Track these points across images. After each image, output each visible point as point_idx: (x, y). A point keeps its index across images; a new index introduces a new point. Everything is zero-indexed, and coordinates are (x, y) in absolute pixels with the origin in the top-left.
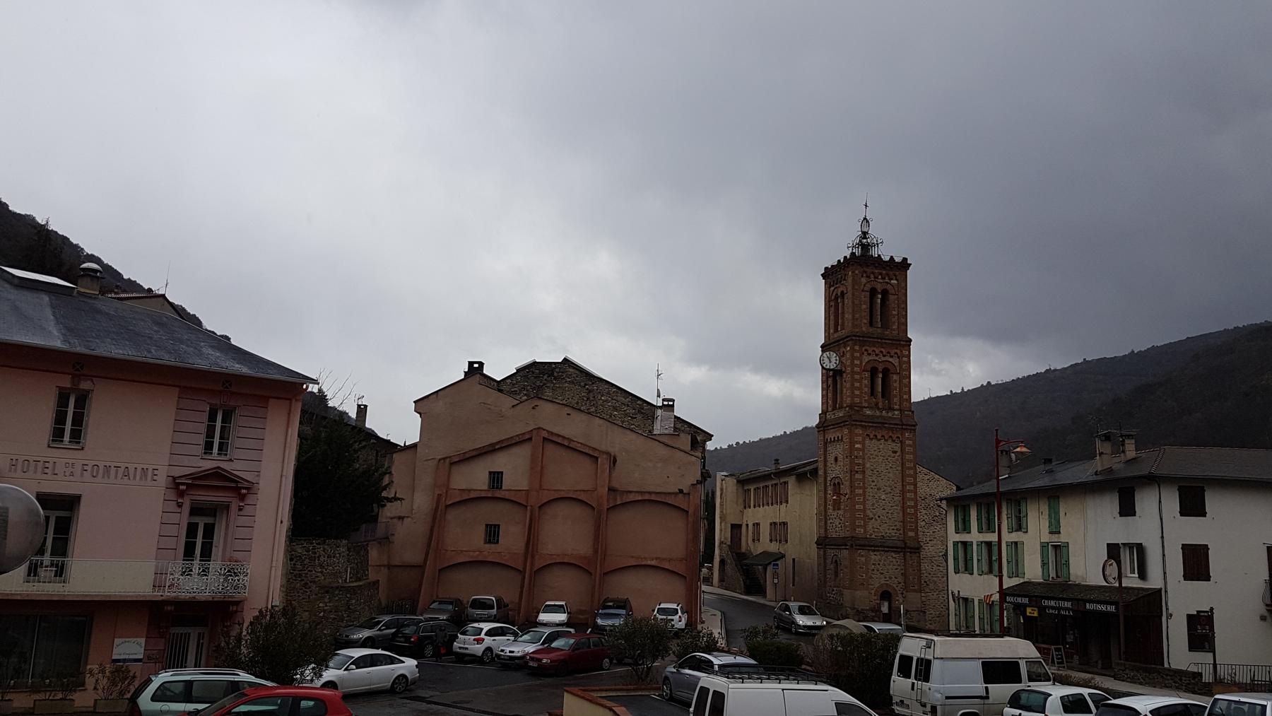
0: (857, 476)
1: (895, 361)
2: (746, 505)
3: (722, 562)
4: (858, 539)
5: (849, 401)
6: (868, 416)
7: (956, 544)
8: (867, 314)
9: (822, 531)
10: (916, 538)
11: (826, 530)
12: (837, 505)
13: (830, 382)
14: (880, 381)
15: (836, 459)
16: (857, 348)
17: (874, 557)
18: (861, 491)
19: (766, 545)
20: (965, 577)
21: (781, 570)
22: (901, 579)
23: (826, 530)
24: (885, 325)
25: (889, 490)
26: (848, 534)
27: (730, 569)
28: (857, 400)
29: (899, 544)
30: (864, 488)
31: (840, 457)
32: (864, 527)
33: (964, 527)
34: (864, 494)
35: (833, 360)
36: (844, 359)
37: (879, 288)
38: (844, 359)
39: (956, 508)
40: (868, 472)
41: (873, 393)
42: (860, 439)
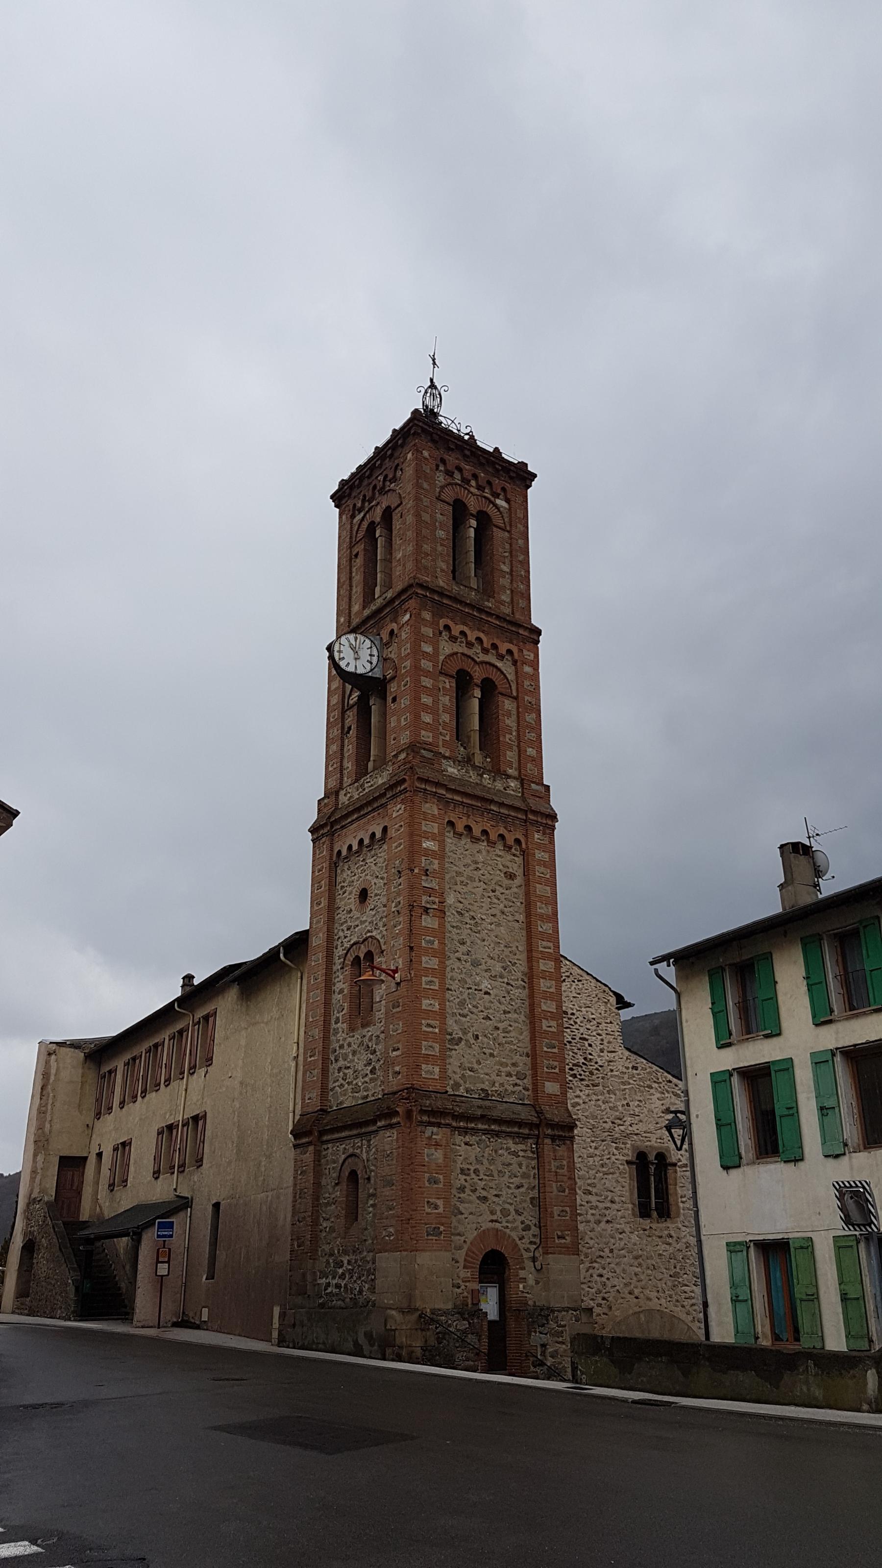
0: (428, 922)
1: (506, 667)
2: (101, 1109)
3: (29, 1248)
4: (427, 1094)
5: (405, 739)
6: (452, 779)
7: (720, 1080)
8: (444, 550)
9: (315, 1094)
10: (561, 1100)
11: (324, 1090)
12: (361, 1010)
13: (351, 718)
14: (476, 703)
15: (363, 895)
16: (427, 615)
17: (468, 1150)
18: (434, 963)
19: (146, 1187)
20: (772, 1173)
21: (179, 1239)
22: (529, 1217)
23: (324, 1090)
24: (488, 589)
25: (498, 968)
26: (395, 1083)
27: (42, 1263)
28: (426, 736)
29: (526, 1114)
30: (442, 955)
31: (376, 887)
32: (442, 1060)
33: (755, 1016)
34: (441, 973)
35: (365, 654)
36: (392, 653)
37: (473, 504)
38: (392, 653)
39: (715, 977)
40: (451, 918)
41: (460, 733)
42: (434, 828)
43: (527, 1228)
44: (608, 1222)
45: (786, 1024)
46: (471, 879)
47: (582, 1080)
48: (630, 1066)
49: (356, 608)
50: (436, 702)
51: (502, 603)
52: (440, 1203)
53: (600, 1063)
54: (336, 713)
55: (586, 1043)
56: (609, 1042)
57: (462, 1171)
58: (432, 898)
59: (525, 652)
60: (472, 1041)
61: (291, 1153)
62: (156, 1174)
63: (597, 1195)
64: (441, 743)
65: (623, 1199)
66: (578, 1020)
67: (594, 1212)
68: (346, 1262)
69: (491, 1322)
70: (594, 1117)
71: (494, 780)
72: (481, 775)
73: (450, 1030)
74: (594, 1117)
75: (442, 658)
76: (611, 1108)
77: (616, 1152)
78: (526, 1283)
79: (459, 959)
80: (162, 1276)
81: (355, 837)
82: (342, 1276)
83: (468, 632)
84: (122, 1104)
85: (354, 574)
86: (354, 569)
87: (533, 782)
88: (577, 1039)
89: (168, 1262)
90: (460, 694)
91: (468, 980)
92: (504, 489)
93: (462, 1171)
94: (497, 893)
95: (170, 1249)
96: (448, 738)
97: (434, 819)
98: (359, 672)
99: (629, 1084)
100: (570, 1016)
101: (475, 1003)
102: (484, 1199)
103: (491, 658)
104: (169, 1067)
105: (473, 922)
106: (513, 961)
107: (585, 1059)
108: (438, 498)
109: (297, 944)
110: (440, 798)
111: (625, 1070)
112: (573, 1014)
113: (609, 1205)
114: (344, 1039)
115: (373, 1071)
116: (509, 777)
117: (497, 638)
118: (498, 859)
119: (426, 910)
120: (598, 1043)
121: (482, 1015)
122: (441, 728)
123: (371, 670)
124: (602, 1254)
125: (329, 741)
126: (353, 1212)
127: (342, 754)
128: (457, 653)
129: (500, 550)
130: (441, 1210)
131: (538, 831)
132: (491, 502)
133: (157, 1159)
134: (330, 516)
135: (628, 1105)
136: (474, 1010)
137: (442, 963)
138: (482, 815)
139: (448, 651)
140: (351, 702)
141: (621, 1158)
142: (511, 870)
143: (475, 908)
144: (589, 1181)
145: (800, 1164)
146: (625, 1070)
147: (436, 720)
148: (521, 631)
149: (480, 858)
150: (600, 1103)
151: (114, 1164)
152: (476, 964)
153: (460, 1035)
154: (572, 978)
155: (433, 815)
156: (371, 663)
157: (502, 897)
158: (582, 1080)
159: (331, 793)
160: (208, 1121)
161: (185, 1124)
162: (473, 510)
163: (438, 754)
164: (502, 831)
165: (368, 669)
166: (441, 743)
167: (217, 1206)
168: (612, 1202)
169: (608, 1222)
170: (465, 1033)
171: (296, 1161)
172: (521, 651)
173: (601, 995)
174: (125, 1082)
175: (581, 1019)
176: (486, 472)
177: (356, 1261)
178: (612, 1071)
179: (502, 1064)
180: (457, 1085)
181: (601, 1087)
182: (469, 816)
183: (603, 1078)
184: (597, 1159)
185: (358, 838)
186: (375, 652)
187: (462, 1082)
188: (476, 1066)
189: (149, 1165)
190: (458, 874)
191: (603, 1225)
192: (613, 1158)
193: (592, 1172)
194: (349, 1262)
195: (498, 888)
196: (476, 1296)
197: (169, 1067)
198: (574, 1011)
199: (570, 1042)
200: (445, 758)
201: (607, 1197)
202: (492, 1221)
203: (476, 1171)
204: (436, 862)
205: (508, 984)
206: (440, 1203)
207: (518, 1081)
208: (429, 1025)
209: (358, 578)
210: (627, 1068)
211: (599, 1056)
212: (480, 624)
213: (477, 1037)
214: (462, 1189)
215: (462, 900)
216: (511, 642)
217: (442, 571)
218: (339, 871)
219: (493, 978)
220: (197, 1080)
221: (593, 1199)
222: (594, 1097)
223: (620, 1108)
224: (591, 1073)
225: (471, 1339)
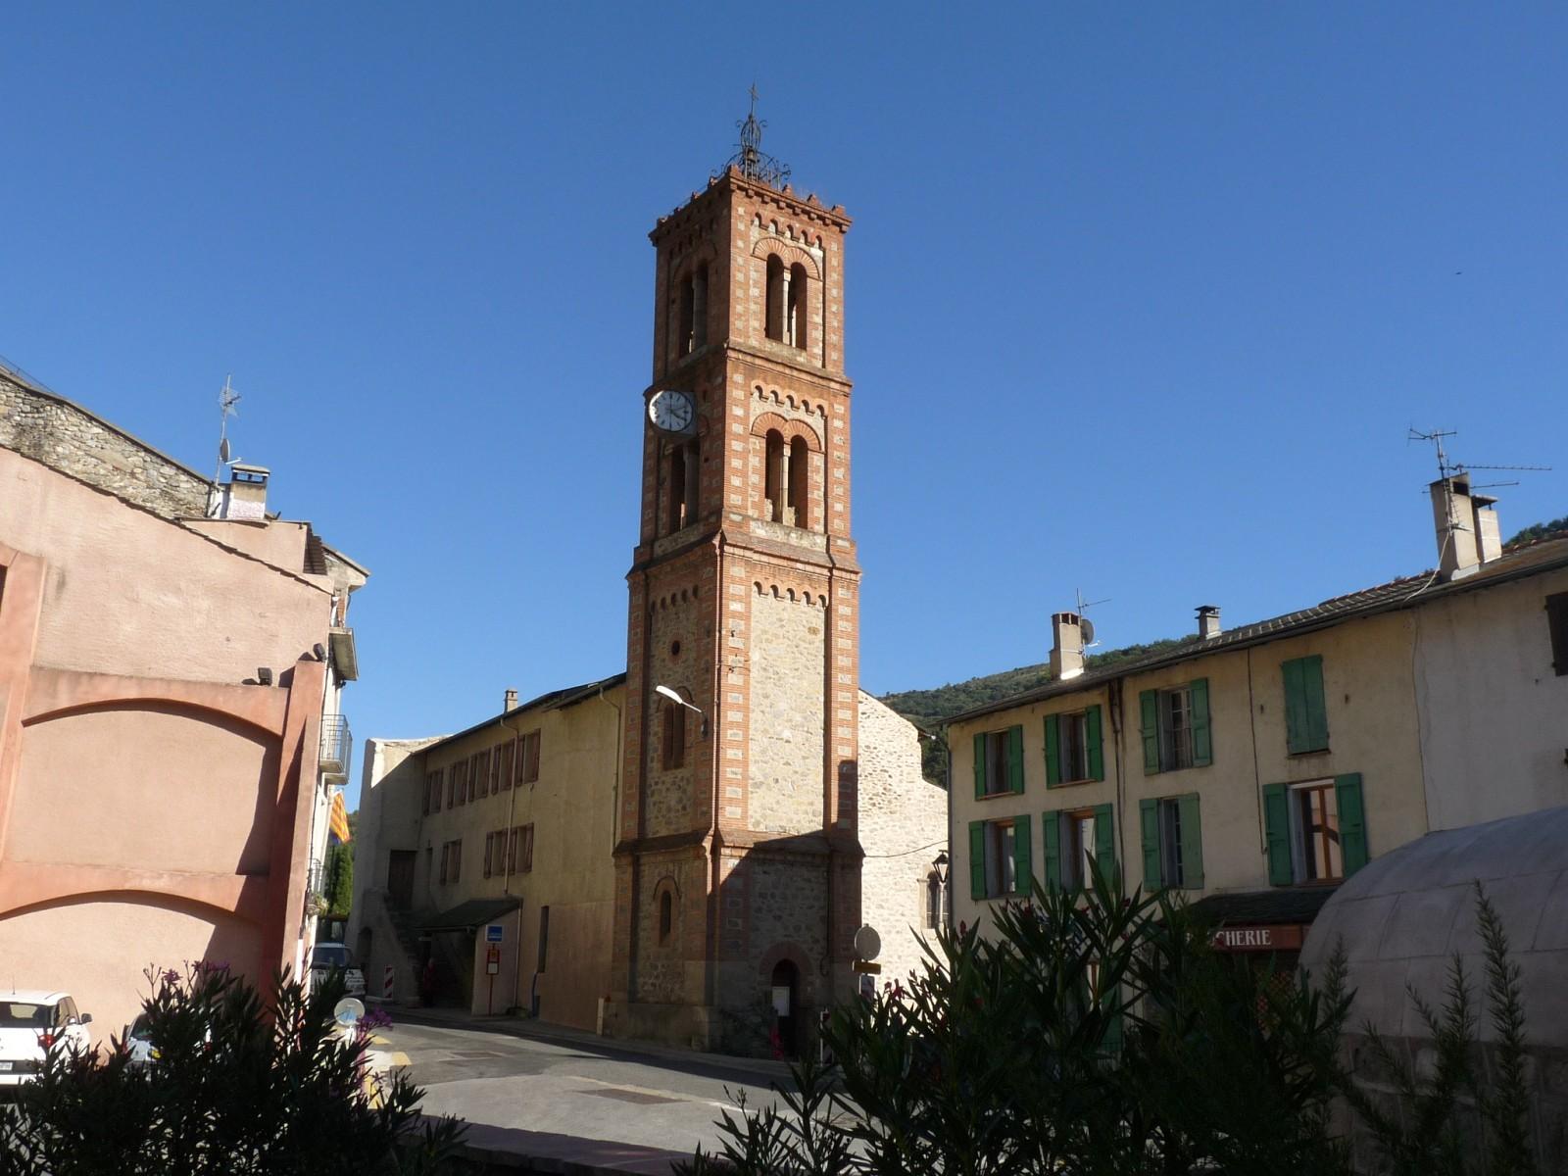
6: (761, 541)
9: (633, 823)
15: (676, 648)
25: (798, 718)
30: (745, 709)
32: (744, 802)
40: (755, 673)
43: (817, 941)
44: (898, 932)
45: (1028, 785)
46: (776, 636)
47: (881, 808)
48: (927, 794)
49: (672, 356)
50: (745, 465)
51: (814, 356)
52: (740, 921)
53: (898, 793)
54: (651, 462)
55: (887, 775)
56: (909, 774)
57: (761, 895)
58: (738, 657)
59: (836, 406)
60: (773, 784)
61: (613, 871)
62: (488, 874)
63: (888, 909)
64: (749, 504)
65: (912, 912)
66: (880, 754)
67: (885, 923)
68: (660, 966)
69: (782, 1019)
70: (890, 841)
71: (801, 539)
72: (788, 535)
73: (753, 776)
74: (890, 841)
75: (752, 419)
76: (907, 833)
77: (908, 872)
78: (813, 985)
79: (763, 712)
80: (492, 974)
81: (669, 590)
82: (657, 977)
83: (779, 392)
84: (450, 805)
85: (670, 320)
86: (671, 315)
87: (839, 538)
88: (878, 772)
89: (498, 962)
90: (771, 450)
91: (771, 731)
92: (819, 238)
93: (761, 895)
94: (801, 648)
95: (498, 951)
96: (756, 500)
97: (741, 581)
98: (673, 429)
99: (925, 810)
100: (872, 750)
101: (775, 751)
102: (779, 918)
103: (801, 414)
104: (496, 777)
105: (776, 677)
106: (814, 711)
107: (885, 789)
108: (753, 255)
109: (619, 680)
110: (747, 561)
111: (922, 799)
112: (875, 748)
113: (900, 917)
114: (659, 778)
115: (684, 808)
116: (815, 534)
117: (809, 394)
118: (803, 615)
119: (731, 669)
120: (898, 775)
121: (782, 761)
122: (750, 489)
123: (686, 427)
124: (890, 959)
125: (645, 490)
126: (666, 925)
127: (658, 505)
128: (767, 413)
129: (814, 301)
130: (740, 928)
131: (842, 587)
132: (805, 252)
133: (487, 860)
134: (648, 256)
135: (923, 829)
136: (776, 757)
137: (746, 716)
138: (788, 574)
139: (758, 412)
140: (666, 453)
141: (913, 876)
142: (814, 625)
143: (778, 664)
144: (883, 898)
145: (1553, 672)
146: (922, 799)
147: (745, 483)
148: (833, 385)
149: (785, 615)
150: (897, 828)
151: (444, 863)
152: (776, 716)
153: (762, 779)
154: (876, 714)
155: (741, 578)
156: (685, 420)
157: (805, 652)
158: (881, 808)
159: (648, 541)
160: (535, 832)
161: (515, 832)
162: (787, 263)
163: (746, 518)
164: (807, 588)
165: (683, 426)
166: (749, 504)
167: (546, 908)
168: (903, 915)
169: (898, 932)
170: (766, 778)
171: (617, 879)
172: (831, 405)
173: (903, 730)
174: (451, 787)
175: (883, 752)
176: (801, 222)
177: (668, 966)
178: (909, 799)
179: (799, 804)
180: (758, 823)
181: (898, 815)
182: (775, 577)
183: (901, 806)
184: (891, 878)
185: (671, 592)
186: (689, 409)
187: (762, 820)
188: (775, 806)
189: (479, 866)
190: (765, 632)
191: (893, 935)
192: (906, 877)
193: (885, 890)
194: (663, 966)
195: (801, 643)
196: (768, 996)
197: (496, 777)
198: (877, 746)
199: (871, 774)
200: (754, 520)
201: (897, 911)
202: (786, 936)
203: (773, 896)
204: (743, 622)
205: (808, 732)
206: (740, 921)
207: (814, 819)
208: (733, 773)
209: (674, 325)
210: (925, 796)
211: (898, 786)
212: (791, 382)
213: (777, 781)
214: (759, 910)
215: (767, 657)
216: (821, 397)
217: (755, 329)
218: (653, 622)
219: (794, 728)
220: (524, 793)
221: (885, 912)
222: (891, 824)
223: (915, 833)
224: (890, 802)
225: (764, 1031)
